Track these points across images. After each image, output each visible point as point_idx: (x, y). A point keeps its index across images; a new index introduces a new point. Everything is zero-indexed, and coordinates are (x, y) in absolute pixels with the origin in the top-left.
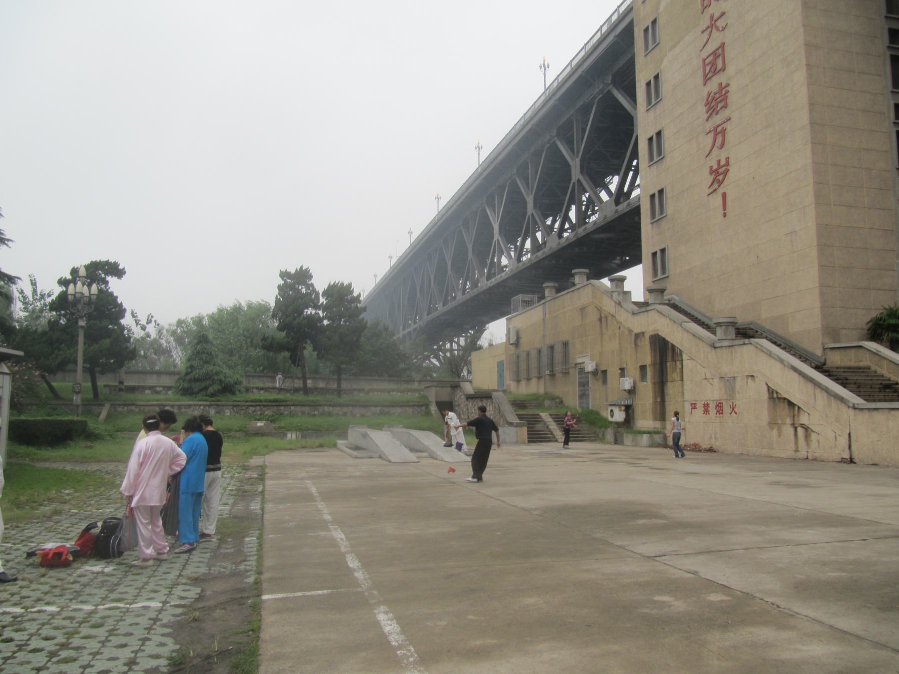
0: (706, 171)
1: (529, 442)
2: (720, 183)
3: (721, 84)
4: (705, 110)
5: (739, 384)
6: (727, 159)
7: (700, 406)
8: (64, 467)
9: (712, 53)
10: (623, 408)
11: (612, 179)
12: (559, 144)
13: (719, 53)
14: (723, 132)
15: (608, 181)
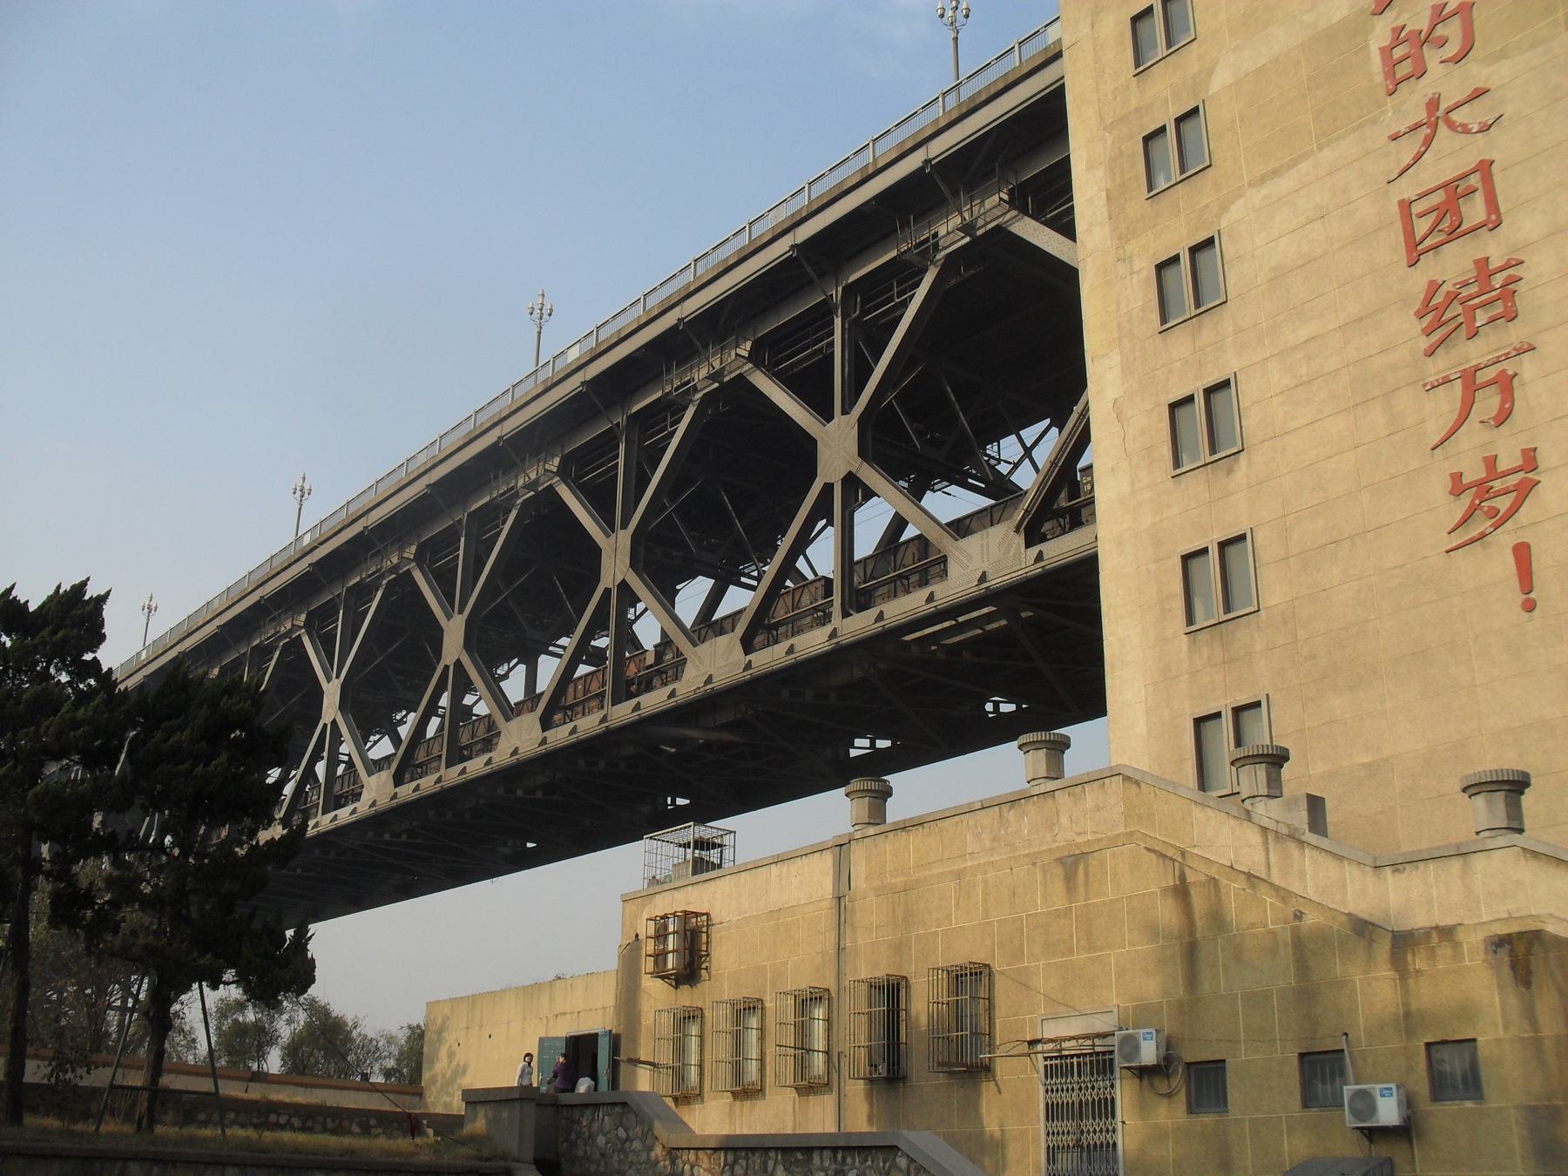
0: (1438, 487)
6: (1530, 460)
8: (1286, 945)
9: (1445, 186)
11: (405, 716)
12: (418, 576)
14: (1506, 384)
15: (398, 717)
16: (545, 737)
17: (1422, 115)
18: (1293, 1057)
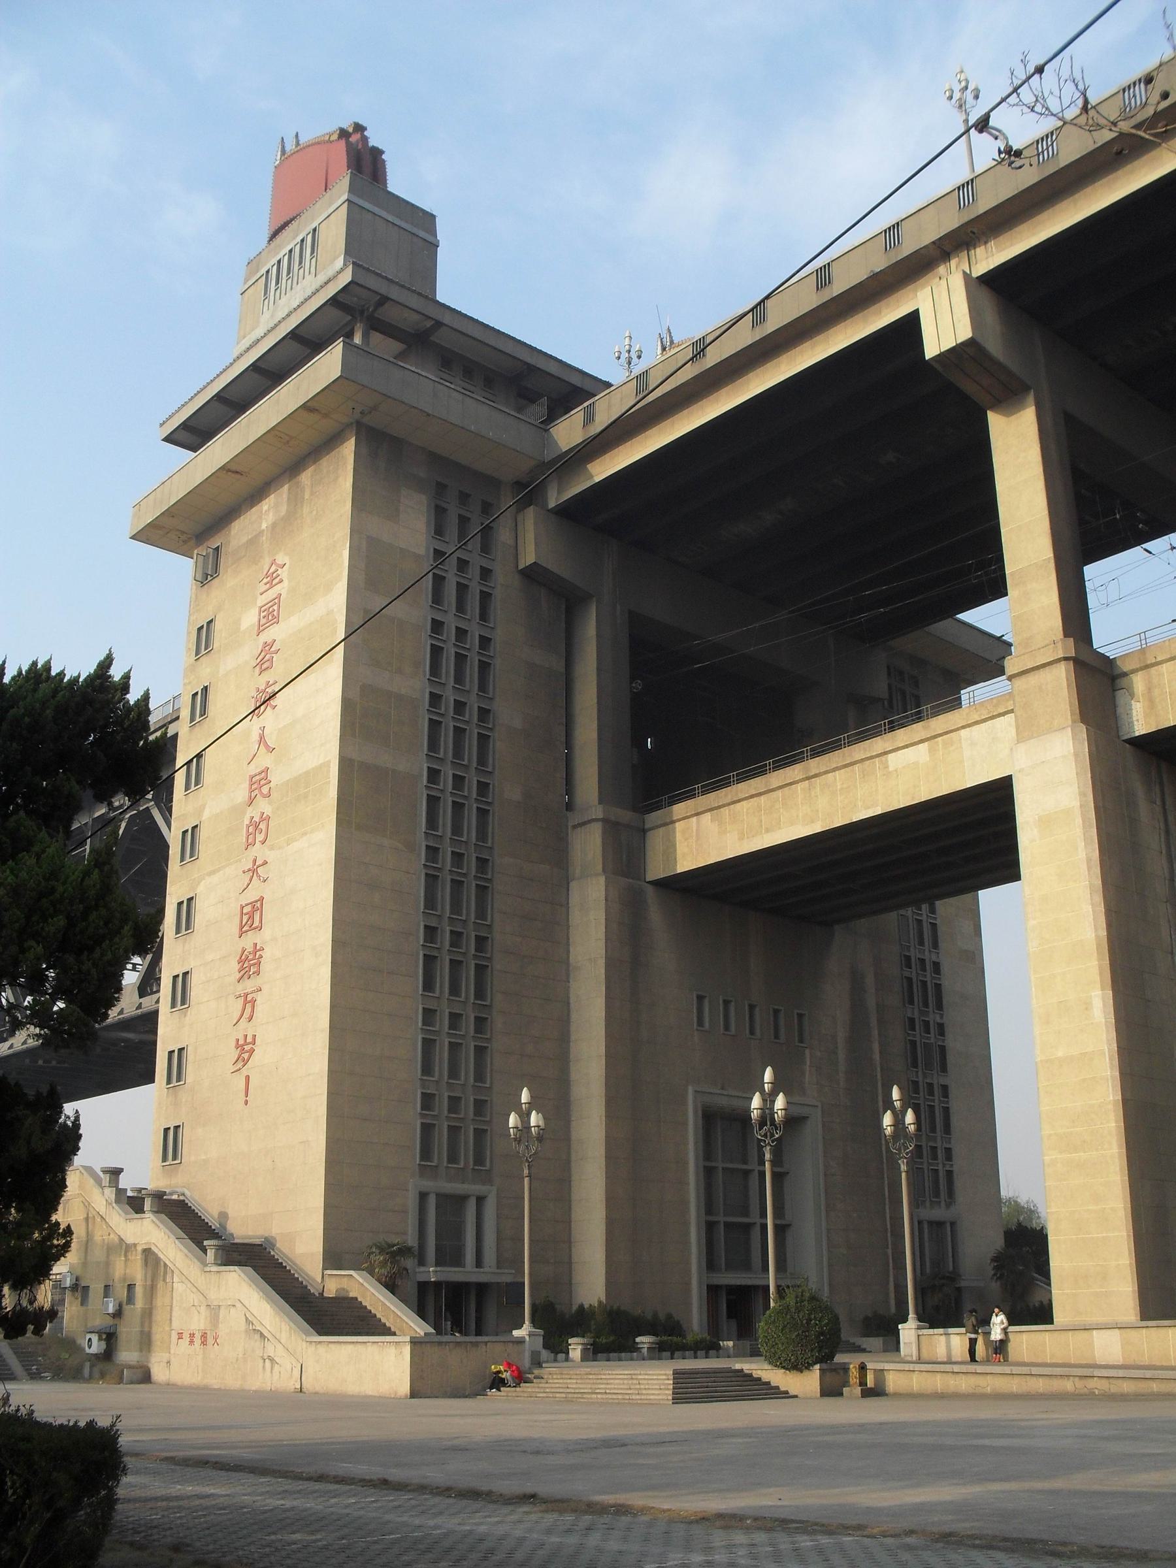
1: (862, 1397)
2: (246, 1062)
3: (256, 945)
4: (237, 969)
5: (222, 1312)
7: (186, 1336)
10: (104, 1336)
13: (257, 906)
14: (253, 1001)
16: (141, 1003)
17: (250, 866)
18: (103, 1286)
